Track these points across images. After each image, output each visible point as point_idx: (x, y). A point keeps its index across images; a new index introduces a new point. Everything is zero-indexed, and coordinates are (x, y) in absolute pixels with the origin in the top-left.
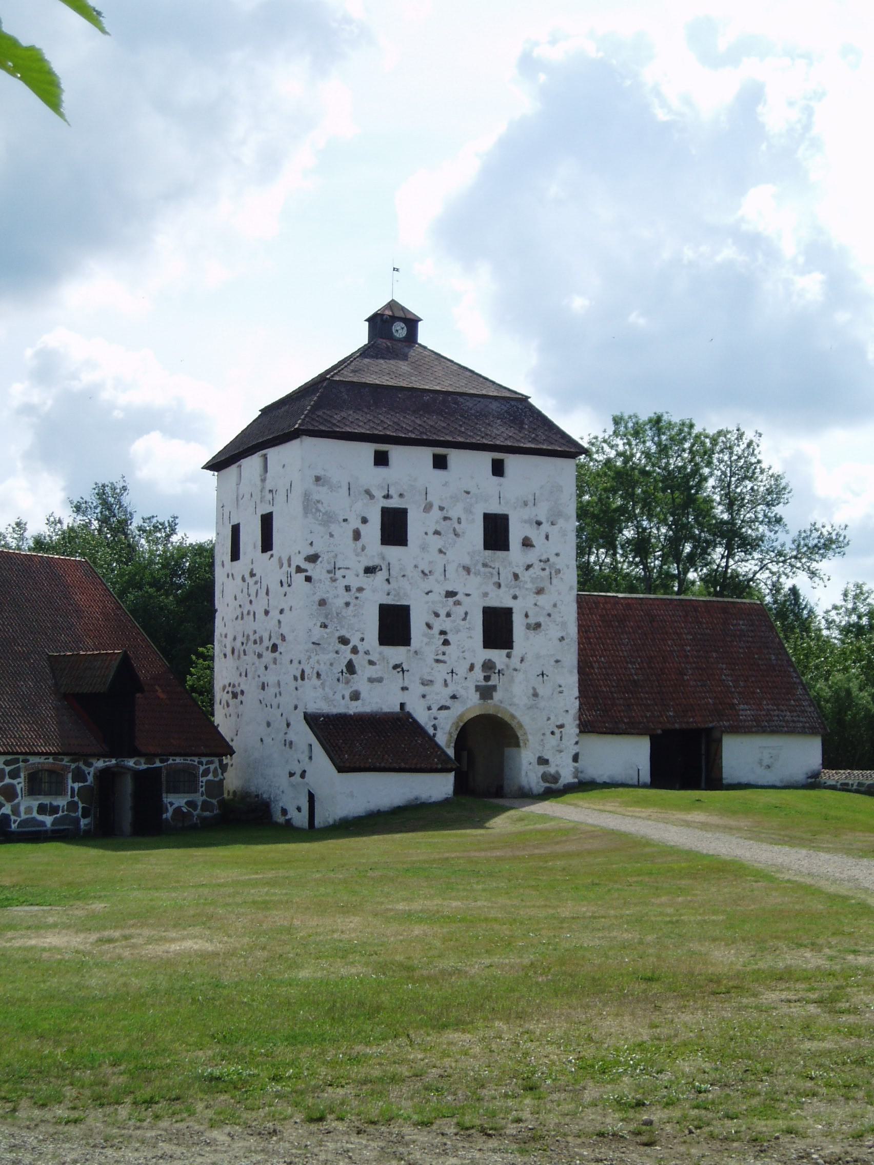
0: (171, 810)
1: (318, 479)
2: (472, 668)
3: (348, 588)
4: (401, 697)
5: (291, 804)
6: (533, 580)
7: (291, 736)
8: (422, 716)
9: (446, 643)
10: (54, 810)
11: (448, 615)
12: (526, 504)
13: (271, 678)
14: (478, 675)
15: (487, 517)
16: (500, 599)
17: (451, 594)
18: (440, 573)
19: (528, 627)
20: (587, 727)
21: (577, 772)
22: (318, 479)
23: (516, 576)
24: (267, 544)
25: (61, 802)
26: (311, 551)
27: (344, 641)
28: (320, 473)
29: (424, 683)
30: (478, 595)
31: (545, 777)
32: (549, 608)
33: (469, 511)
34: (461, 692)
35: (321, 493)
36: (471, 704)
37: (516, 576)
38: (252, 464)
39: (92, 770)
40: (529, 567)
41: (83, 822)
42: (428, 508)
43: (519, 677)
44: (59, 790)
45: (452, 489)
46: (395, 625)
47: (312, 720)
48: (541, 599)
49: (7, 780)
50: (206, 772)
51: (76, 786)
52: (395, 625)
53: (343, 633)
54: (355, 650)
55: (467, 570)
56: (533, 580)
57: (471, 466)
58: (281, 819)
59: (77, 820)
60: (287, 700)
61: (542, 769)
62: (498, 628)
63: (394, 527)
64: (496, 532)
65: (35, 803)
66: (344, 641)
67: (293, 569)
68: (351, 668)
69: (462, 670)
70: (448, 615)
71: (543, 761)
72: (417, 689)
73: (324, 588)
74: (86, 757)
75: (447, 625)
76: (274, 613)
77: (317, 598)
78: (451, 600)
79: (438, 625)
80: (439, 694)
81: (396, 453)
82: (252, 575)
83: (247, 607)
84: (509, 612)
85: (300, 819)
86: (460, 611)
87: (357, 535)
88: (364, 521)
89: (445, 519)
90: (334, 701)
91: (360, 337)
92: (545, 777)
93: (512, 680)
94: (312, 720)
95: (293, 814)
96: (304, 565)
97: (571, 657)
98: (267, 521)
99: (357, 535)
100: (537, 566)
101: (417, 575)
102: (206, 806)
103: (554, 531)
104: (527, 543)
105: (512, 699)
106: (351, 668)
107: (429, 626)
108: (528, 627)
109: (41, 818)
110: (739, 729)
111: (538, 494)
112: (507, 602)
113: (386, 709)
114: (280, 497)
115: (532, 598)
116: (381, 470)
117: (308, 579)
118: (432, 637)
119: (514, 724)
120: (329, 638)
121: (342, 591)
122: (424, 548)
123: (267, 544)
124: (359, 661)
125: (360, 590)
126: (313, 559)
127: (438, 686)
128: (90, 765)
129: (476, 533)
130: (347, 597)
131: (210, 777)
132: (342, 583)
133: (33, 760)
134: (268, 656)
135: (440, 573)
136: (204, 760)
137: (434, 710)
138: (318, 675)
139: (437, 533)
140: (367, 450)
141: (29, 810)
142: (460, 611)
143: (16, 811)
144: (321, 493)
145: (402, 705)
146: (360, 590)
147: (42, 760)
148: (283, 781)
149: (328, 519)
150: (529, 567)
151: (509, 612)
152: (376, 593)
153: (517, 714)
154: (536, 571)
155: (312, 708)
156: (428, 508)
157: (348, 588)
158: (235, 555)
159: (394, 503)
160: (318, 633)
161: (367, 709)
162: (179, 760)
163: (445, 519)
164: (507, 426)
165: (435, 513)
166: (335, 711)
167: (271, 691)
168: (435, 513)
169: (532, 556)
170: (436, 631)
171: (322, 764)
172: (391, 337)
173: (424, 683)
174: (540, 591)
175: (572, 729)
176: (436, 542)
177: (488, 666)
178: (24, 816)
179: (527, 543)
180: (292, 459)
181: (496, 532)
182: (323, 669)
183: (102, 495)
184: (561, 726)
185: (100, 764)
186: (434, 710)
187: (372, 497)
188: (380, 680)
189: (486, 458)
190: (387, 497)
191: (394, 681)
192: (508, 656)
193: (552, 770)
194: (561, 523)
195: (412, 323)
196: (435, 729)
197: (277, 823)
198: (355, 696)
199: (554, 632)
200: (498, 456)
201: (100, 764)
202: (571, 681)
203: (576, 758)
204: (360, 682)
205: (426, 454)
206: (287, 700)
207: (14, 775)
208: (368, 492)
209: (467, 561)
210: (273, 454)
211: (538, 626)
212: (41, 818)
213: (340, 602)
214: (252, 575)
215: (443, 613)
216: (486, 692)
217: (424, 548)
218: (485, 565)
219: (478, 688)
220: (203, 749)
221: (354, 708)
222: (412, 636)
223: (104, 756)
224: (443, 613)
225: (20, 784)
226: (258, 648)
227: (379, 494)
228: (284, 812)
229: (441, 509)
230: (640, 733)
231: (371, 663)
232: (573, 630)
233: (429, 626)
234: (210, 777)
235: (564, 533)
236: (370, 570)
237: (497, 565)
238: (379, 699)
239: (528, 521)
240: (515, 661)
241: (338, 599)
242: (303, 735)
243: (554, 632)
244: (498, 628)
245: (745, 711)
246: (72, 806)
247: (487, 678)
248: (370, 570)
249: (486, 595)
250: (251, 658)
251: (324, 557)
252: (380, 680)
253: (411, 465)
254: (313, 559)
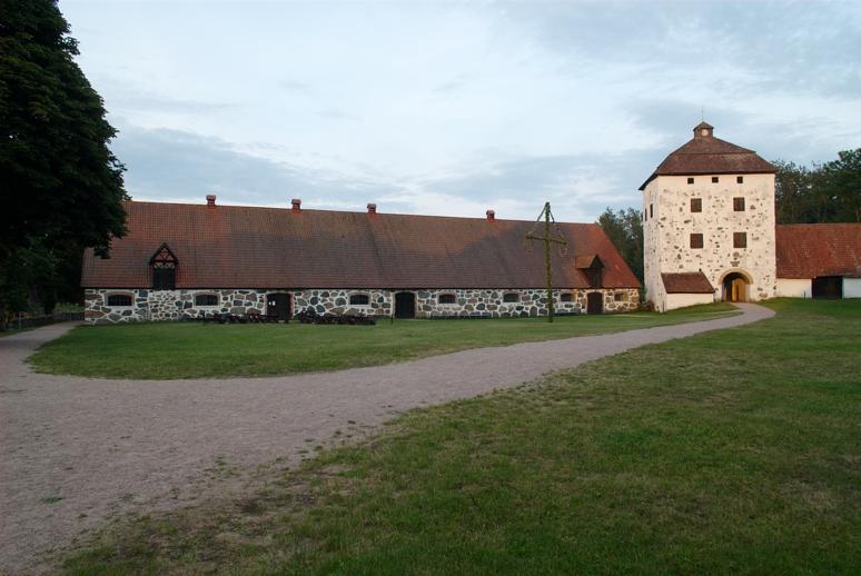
1: (665, 191)
10: (571, 306)
14: (732, 258)
15: (735, 199)
20: (779, 275)
21: (775, 293)
27: (677, 248)
29: (709, 261)
45: (718, 191)
46: (697, 241)
52: (697, 241)
57: (728, 181)
62: (740, 240)
63: (696, 206)
65: (564, 304)
66: (677, 248)
68: (679, 257)
71: (759, 289)
75: (718, 240)
79: (714, 240)
80: (715, 265)
84: (745, 234)
85: (661, 311)
87: (681, 210)
97: (773, 249)
99: (681, 210)
105: (746, 266)
106: (679, 257)
111: (761, 190)
115: (754, 229)
116: (691, 185)
120: (671, 246)
129: (730, 205)
135: (717, 221)
140: (685, 178)
151: (745, 234)
152: (689, 230)
153: (750, 272)
155: (663, 271)
156: (710, 197)
159: (696, 197)
161: (686, 271)
165: (713, 199)
169: (755, 212)
173: (709, 261)
174: (758, 226)
175: (773, 277)
177: (736, 255)
181: (739, 205)
189: (735, 177)
193: (764, 292)
194: (768, 199)
197: (658, 312)
199: (765, 240)
201: (589, 291)
211: (757, 239)
216: (735, 264)
217: (709, 212)
220: (473, 285)
221: (681, 271)
222: (97, 85)
230: (499, 221)
232: (773, 239)
235: (769, 203)
238: (691, 267)
240: (748, 252)
241: (674, 232)
243: (765, 240)
244: (740, 240)
246: (578, 305)
253: (703, 182)
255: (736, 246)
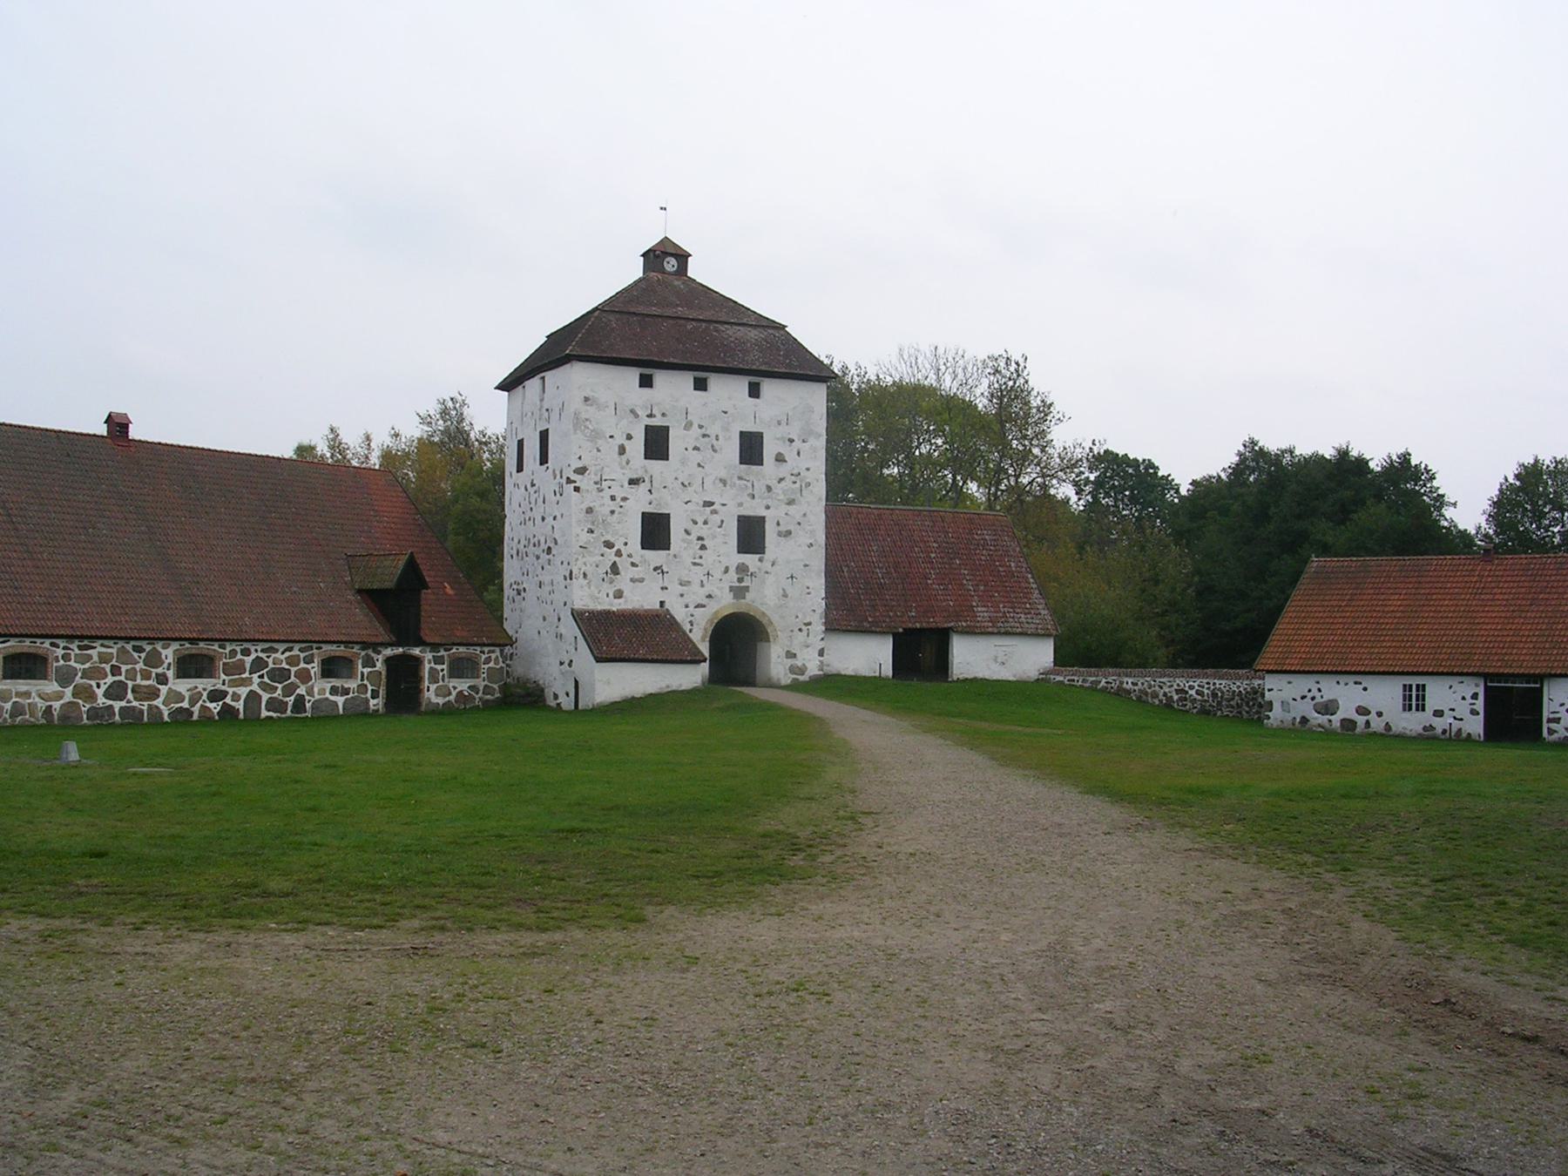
0: (454, 693)
1: (586, 399)
2: (727, 570)
3: (613, 498)
4: (662, 596)
5: (558, 689)
6: (784, 492)
7: (562, 630)
8: (679, 614)
9: (703, 547)
10: (346, 692)
11: (705, 523)
12: (779, 423)
13: (546, 579)
16: (753, 509)
17: (708, 504)
18: (698, 485)
19: (780, 534)
22: (586, 399)
23: (769, 488)
24: (544, 459)
25: (352, 684)
26: (580, 464)
27: (609, 545)
28: (588, 393)
30: (733, 505)
31: (792, 670)
32: (798, 518)
33: (726, 429)
34: (716, 592)
35: (588, 412)
36: (725, 603)
37: (769, 488)
38: (533, 384)
39: (380, 657)
40: (781, 480)
41: (373, 702)
42: (688, 426)
43: (770, 579)
44: (351, 675)
45: (710, 410)
46: (655, 531)
47: (578, 616)
48: (792, 509)
49: (302, 665)
50: (488, 661)
51: (366, 670)
52: (655, 531)
53: (608, 537)
54: (619, 553)
55: (724, 482)
56: (784, 492)
57: (728, 392)
58: (553, 703)
59: (367, 701)
60: (558, 598)
61: (790, 662)
62: (751, 535)
63: (657, 444)
64: (751, 447)
65: (327, 684)
66: (609, 545)
67: (564, 481)
68: (615, 569)
69: (717, 573)
70: (705, 523)
72: (675, 588)
73: (590, 498)
74: (376, 647)
76: (549, 520)
77: (584, 506)
78: (708, 509)
81: (660, 377)
82: (533, 485)
83: (529, 514)
84: (665, 518)
85: (567, 703)
86: (716, 519)
87: (622, 450)
88: (629, 437)
89: (704, 436)
90: (593, 596)
91: (634, 271)
92: (792, 670)
93: (763, 582)
94: (578, 616)
95: (562, 699)
96: (573, 477)
97: (818, 562)
98: (544, 436)
99: (622, 450)
100: (790, 479)
101: (678, 485)
102: (487, 690)
103: (805, 447)
104: (780, 459)
105: (764, 599)
106: (615, 569)
107: (688, 533)
108: (780, 534)
109: (332, 698)
110: (970, 632)
111: (794, 417)
112: (762, 512)
113: (647, 607)
114: (555, 416)
116: (646, 391)
117: (577, 489)
118: (689, 542)
119: (764, 621)
121: (607, 500)
122: (683, 462)
123: (544, 459)
124: (623, 563)
125: (624, 499)
126: (581, 471)
127: (695, 587)
128: (379, 653)
129: (732, 449)
130: (613, 505)
131: (492, 664)
132: (607, 493)
133: (325, 647)
134: (544, 557)
136: (486, 649)
137: (691, 608)
138: (585, 575)
139: (696, 448)
141: (322, 691)
142: (716, 519)
143: (310, 692)
144: (588, 412)
145: (662, 603)
146: (624, 499)
147: (334, 647)
148: (555, 669)
149: (595, 435)
150: (781, 480)
152: (639, 503)
154: (786, 484)
156: (688, 426)
157: (613, 498)
158: (520, 469)
160: (585, 537)
161: (629, 606)
162: (462, 649)
163: (704, 436)
164: (771, 355)
166: (599, 608)
167: (547, 588)
168: (695, 430)
169: (783, 471)
170: (693, 537)
171: (583, 656)
172: (663, 271)
174: (791, 502)
176: (696, 457)
177: (742, 569)
178: (317, 697)
179: (780, 459)
180: (578, 378)
181: (751, 447)
182: (589, 569)
183: (444, 413)
184: (809, 624)
185: (389, 652)
186: (691, 608)
187: (637, 416)
188: (641, 580)
190: (650, 416)
191: (654, 582)
192: (761, 560)
195: (683, 257)
196: (691, 623)
198: (619, 594)
200: (755, 379)
201: (389, 652)
202: (818, 584)
203: (821, 653)
204: (623, 582)
205: (687, 379)
206: (558, 598)
207: (309, 660)
208: (632, 411)
209: (723, 474)
210: (548, 375)
211: (789, 533)
212: (332, 698)
213: (606, 510)
214: (533, 485)
215: (700, 520)
216: (739, 592)
218: (740, 478)
219: (731, 589)
221: (616, 605)
223: (391, 645)
224: (700, 520)
225: (315, 668)
226: (538, 551)
227: (642, 413)
228: (556, 696)
229: (701, 427)
231: (633, 564)
232: (821, 538)
233: (688, 533)
234: (492, 664)
236: (633, 482)
237: (751, 478)
238: (640, 598)
239: (781, 439)
240: (767, 565)
241: (603, 506)
242: (570, 628)
243: (802, 538)
244: (751, 535)
245: (983, 613)
246: (362, 688)
247: (740, 580)
248: (633, 482)
249: (740, 505)
250: (531, 558)
251: (592, 469)
252: (641, 580)
253: (673, 389)
254: (581, 471)
255: (649, 454)
